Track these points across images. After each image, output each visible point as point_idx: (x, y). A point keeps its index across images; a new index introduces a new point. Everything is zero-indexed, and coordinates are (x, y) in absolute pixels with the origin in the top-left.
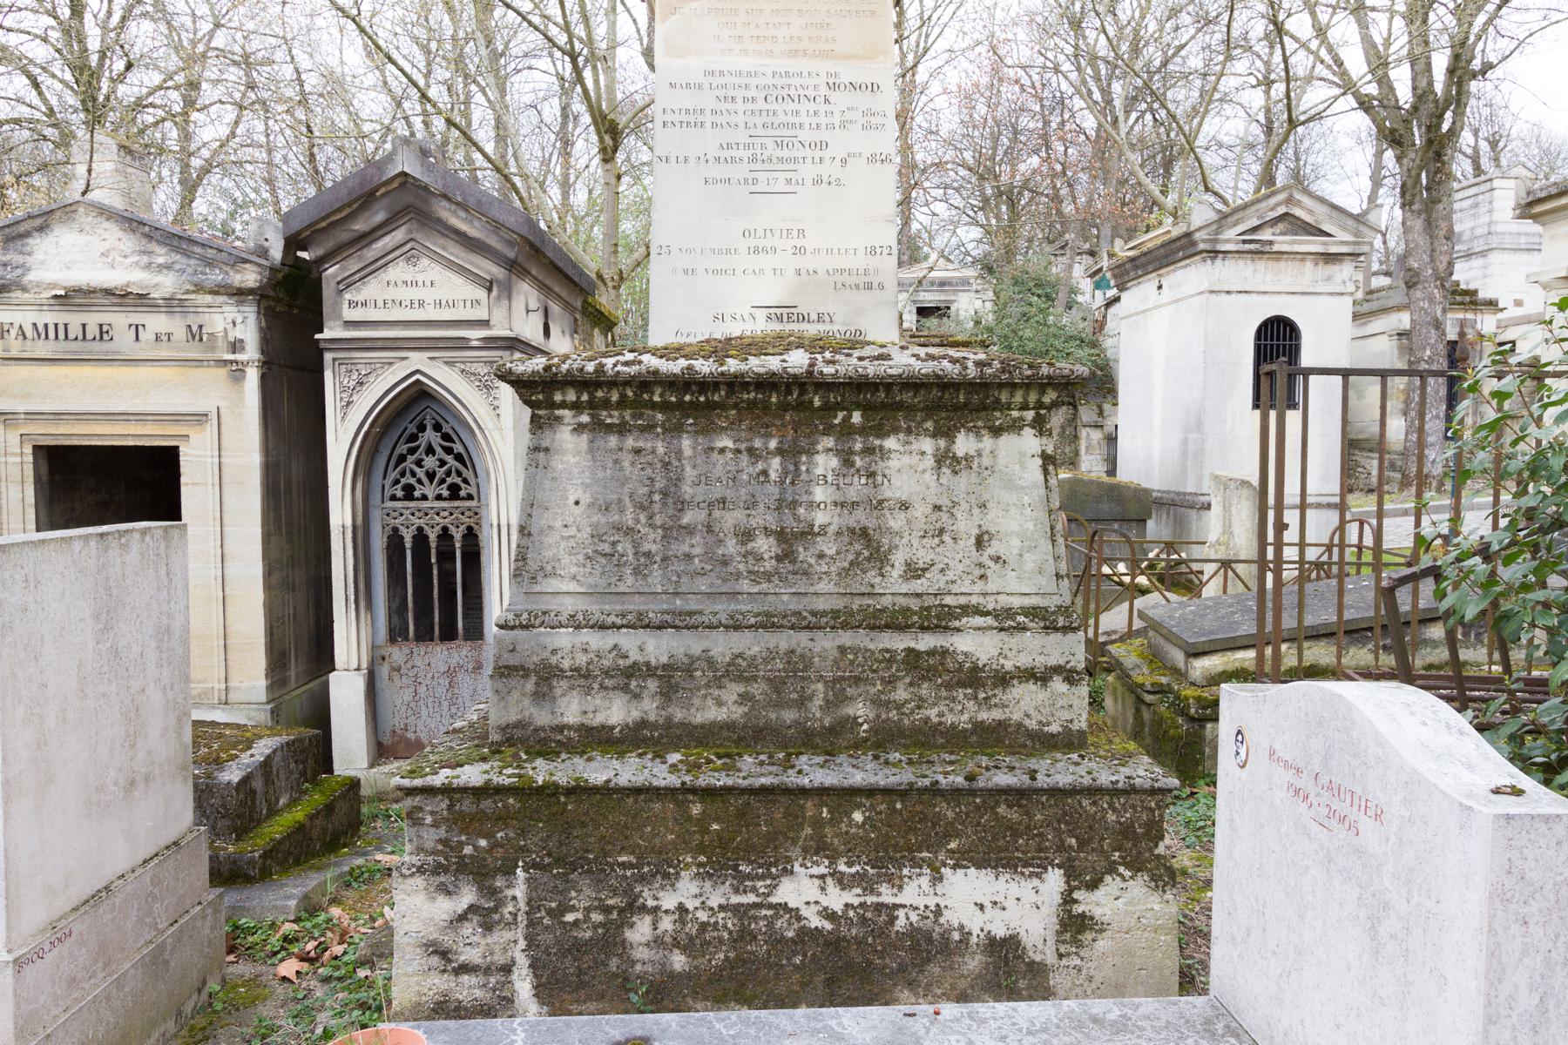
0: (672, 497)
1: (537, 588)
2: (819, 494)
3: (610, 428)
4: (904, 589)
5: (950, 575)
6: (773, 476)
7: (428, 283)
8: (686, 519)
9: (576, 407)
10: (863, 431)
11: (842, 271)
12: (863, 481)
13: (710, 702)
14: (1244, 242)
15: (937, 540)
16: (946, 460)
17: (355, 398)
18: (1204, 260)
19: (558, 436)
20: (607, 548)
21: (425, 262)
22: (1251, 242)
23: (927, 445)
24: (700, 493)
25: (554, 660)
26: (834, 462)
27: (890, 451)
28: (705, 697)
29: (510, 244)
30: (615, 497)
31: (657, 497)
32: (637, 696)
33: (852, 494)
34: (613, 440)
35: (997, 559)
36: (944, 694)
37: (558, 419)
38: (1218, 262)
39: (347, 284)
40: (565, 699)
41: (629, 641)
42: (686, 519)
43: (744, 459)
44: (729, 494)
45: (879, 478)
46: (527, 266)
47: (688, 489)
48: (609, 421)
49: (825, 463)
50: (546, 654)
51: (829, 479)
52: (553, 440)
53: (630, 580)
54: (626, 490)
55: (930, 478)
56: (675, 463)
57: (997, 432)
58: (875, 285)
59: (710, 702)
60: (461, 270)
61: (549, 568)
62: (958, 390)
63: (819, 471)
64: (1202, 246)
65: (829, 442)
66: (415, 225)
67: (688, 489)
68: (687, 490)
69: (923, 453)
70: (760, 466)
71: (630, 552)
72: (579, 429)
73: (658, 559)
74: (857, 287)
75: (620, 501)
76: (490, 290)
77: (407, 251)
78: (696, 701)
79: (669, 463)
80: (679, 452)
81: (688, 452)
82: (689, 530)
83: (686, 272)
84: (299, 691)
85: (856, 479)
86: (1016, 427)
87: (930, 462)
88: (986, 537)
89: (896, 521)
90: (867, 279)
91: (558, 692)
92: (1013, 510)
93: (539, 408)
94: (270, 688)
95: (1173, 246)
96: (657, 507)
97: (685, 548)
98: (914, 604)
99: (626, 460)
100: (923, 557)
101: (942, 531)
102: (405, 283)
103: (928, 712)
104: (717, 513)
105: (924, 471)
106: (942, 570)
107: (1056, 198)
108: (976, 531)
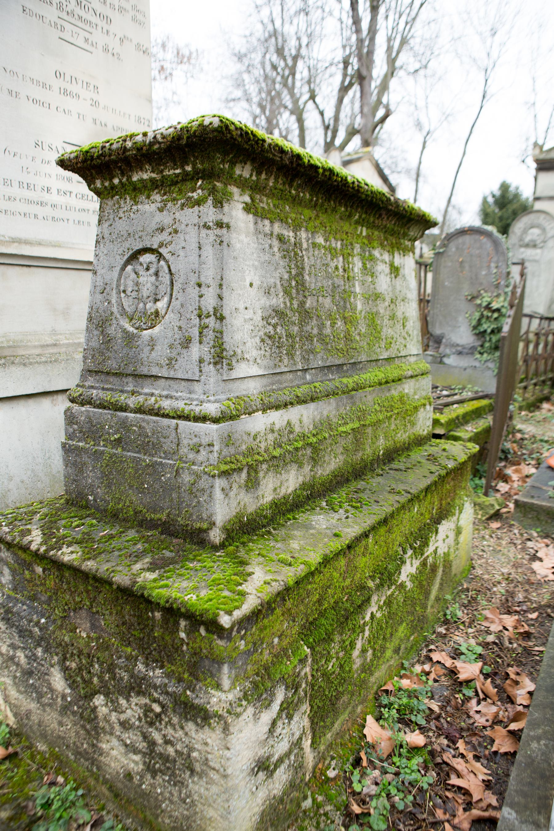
1: (234, 374)
83: (10, 92)
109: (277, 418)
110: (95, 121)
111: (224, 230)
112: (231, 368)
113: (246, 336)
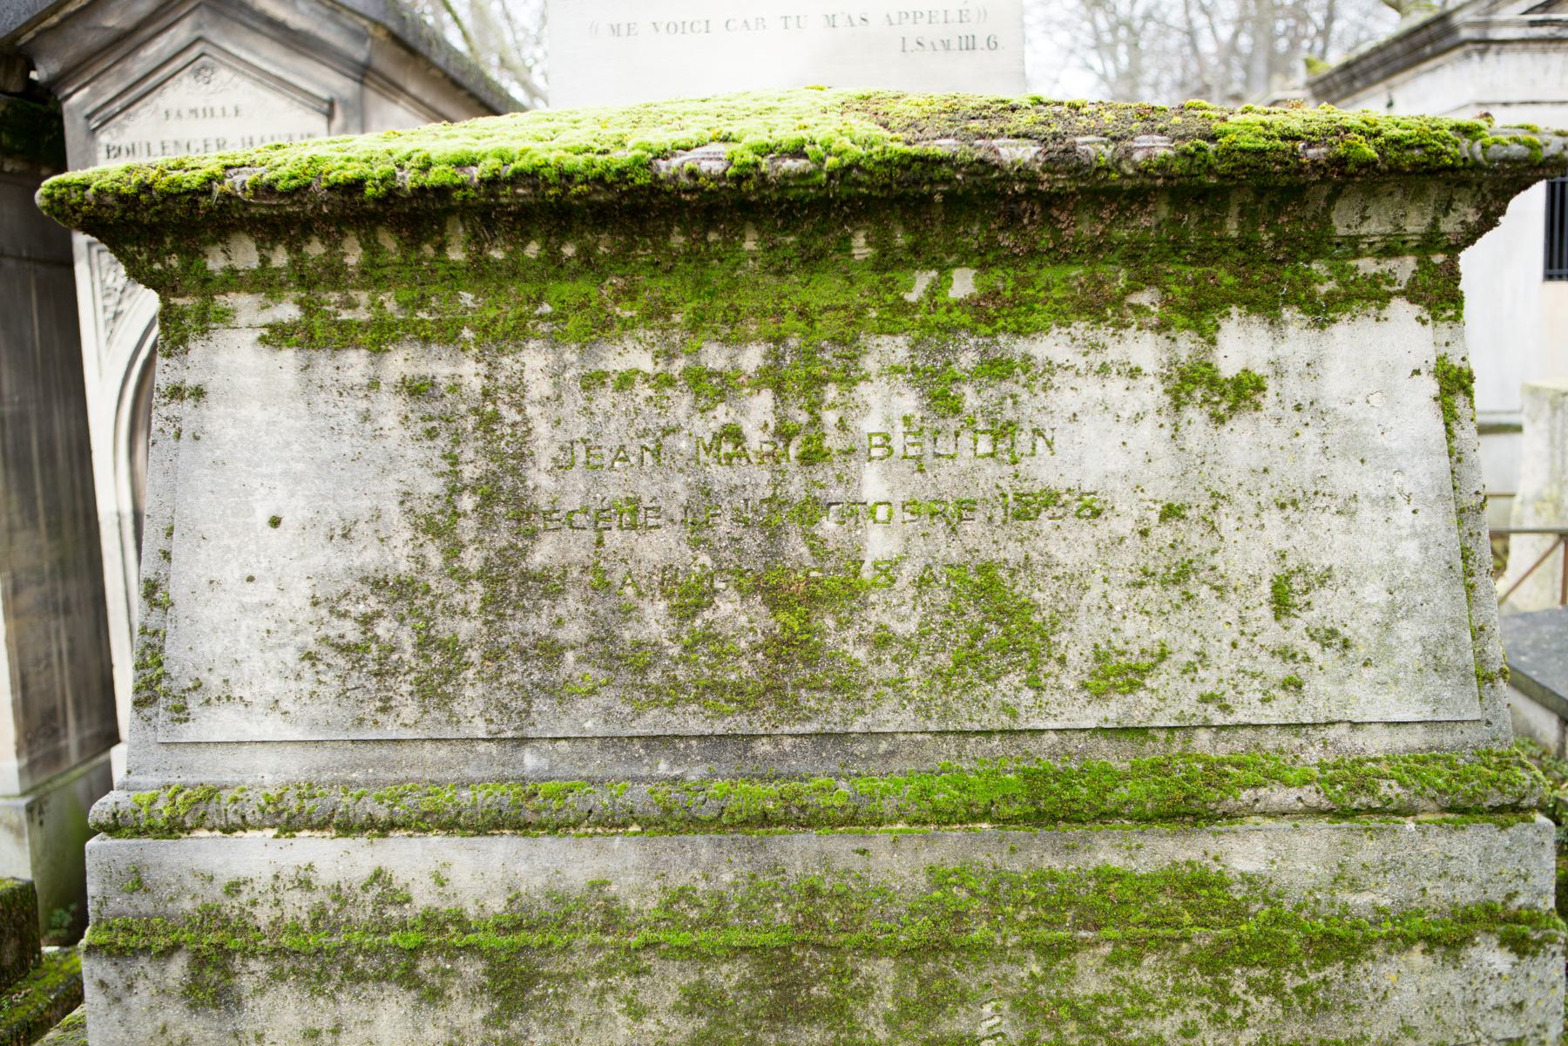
0: (504, 496)
1: (189, 732)
2: (873, 484)
3: (344, 337)
4: (1091, 717)
5: (1209, 680)
6: (756, 440)
7: (230, 111)
8: (542, 554)
9: (265, 283)
10: (983, 310)
11: (916, 16)
12: (984, 446)
13: (614, 1006)
14: (1533, 24)
15: (1175, 593)
16: (1191, 384)
17: (125, 306)
18: (1467, 55)
19: (222, 359)
20: (352, 632)
21: (224, 75)
22: (1542, 23)
23: (1144, 349)
24: (574, 492)
25: (230, 907)
26: (909, 402)
27: (1050, 368)
28: (601, 994)
29: (359, 36)
30: (365, 504)
31: (467, 502)
32: (435, 996)
33: (946, 480)
34: (356, 363)
35: (1327, 637)
36: (1196, 978)
37: (225, 316)
38: (1490, 57)
39: (102, 117)
40: (264, 1002)
41: (412, 860)
42: (542, 554)
43: (681, 404)
44: (646, 490)
45: (1024, 439)
46: (400, 80)
47: (545, 481)
48: (345, 315)
49: (882, 403)
50: (215, 893)
51: (897, 444)
52: (213, 369)
53: (410, 710)
54: (391, 485)
55: (1149, 435)
56: (510, 415)
57: (1321, 313)
58: (981, 42)
59: (614, 1006)
60: (282, 85)
61: (214, 682)
62: (1221, 208)
63: (871, 424)
64: (1465, 33)
65: (897, 349)
66: (206, 16)
67: (545, 481)
68: (540, 480)
69: (1135, 373)
70: (722, 415)
71: (407, 639)
72: (277, 336)
73: (474, 655)
74: (946, 45)
75: (377, 515)
76: (330, 116)
77: (191, 58)
78: (576, 1005)
79: (496, 417)
80: (517, 390)
81: (539, 387)
82: (549, 585)
83: (615, 30)
84: (82, 769)
85: (966, 439)
86: (1375, 295)
87: (1151, 394)
88: (1297, 583)
89: (1065, 544)
90: (965, 30)
91: (246, 983)
92: (1366, 512)
93: (174, 291)
94: (28, 770)
95: (1416, 39)
96: (467, 528)
97: (539, 624)
98: (1115, 757)
99: (390, 408)
100: (1137, 632)
101: (1182, 574)
102: (194, 112)
103: (1156, 1026)
104: (614, 538)
105: (1138, 418)
106: (1189, 669)
107: (1191, 34)
108: (1271, 570)
109: (334, 859)
110: (831, 22)
111: (188, 404)
112: (180, 713)
113: (243, 644)
